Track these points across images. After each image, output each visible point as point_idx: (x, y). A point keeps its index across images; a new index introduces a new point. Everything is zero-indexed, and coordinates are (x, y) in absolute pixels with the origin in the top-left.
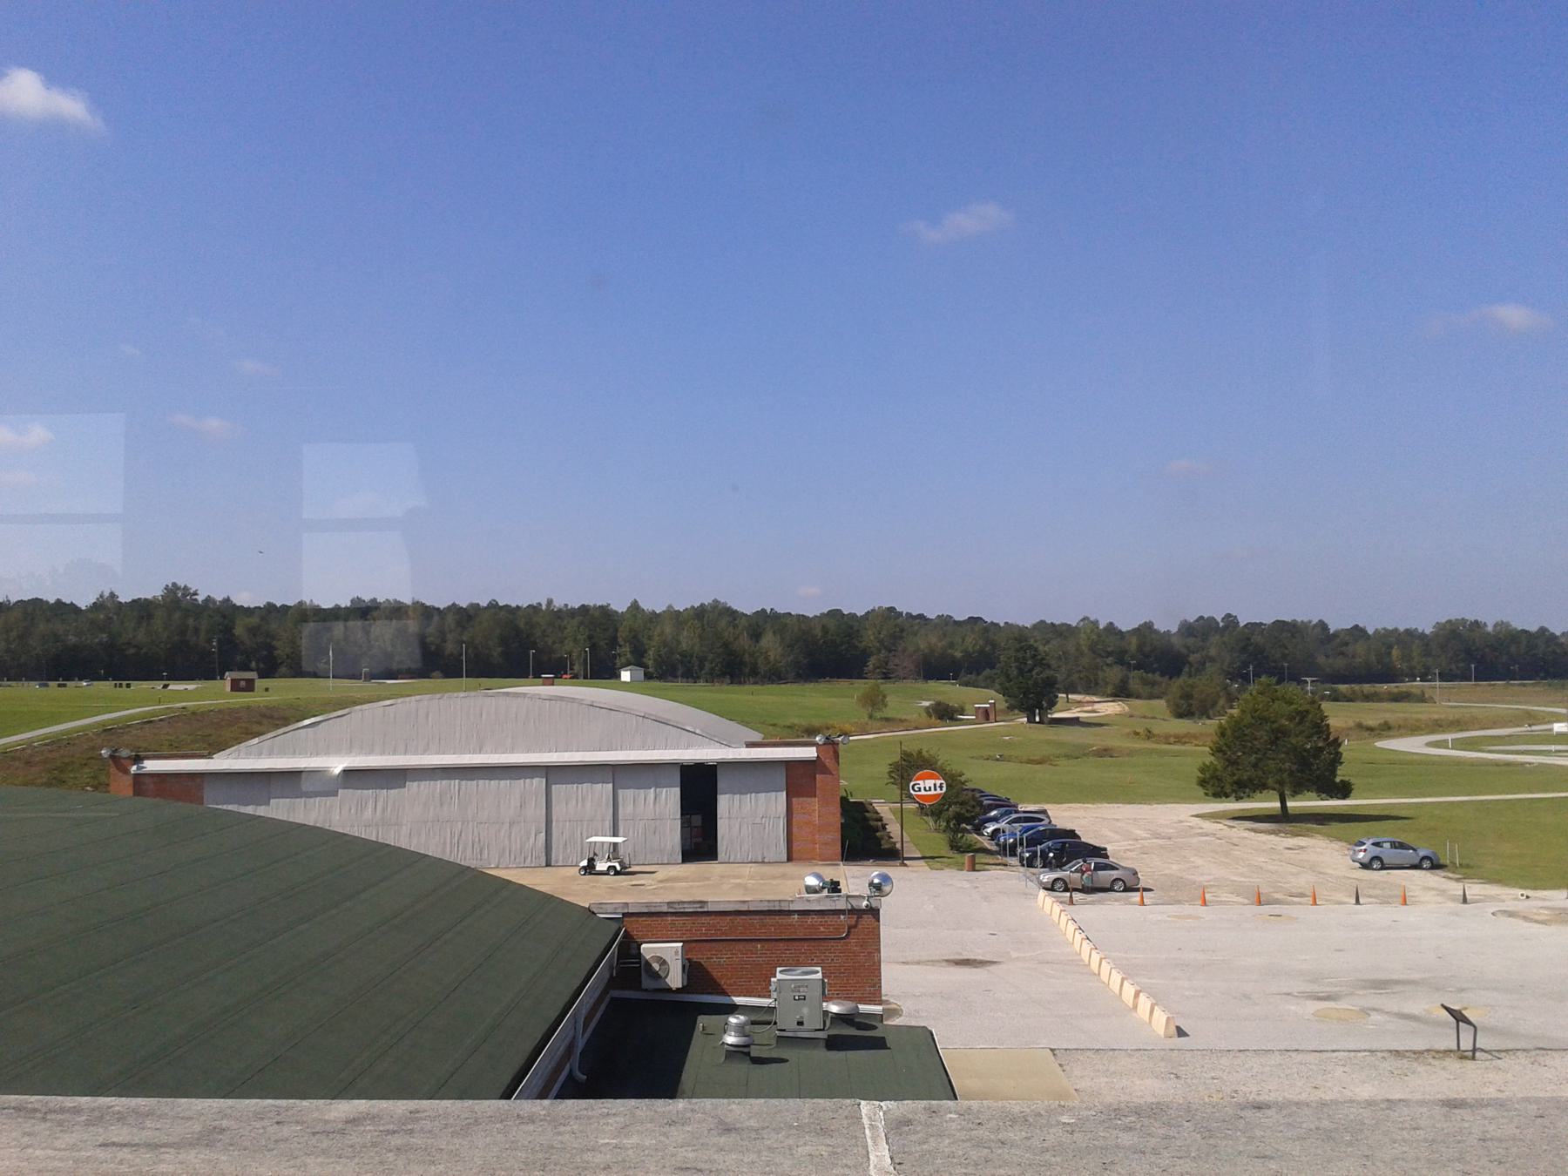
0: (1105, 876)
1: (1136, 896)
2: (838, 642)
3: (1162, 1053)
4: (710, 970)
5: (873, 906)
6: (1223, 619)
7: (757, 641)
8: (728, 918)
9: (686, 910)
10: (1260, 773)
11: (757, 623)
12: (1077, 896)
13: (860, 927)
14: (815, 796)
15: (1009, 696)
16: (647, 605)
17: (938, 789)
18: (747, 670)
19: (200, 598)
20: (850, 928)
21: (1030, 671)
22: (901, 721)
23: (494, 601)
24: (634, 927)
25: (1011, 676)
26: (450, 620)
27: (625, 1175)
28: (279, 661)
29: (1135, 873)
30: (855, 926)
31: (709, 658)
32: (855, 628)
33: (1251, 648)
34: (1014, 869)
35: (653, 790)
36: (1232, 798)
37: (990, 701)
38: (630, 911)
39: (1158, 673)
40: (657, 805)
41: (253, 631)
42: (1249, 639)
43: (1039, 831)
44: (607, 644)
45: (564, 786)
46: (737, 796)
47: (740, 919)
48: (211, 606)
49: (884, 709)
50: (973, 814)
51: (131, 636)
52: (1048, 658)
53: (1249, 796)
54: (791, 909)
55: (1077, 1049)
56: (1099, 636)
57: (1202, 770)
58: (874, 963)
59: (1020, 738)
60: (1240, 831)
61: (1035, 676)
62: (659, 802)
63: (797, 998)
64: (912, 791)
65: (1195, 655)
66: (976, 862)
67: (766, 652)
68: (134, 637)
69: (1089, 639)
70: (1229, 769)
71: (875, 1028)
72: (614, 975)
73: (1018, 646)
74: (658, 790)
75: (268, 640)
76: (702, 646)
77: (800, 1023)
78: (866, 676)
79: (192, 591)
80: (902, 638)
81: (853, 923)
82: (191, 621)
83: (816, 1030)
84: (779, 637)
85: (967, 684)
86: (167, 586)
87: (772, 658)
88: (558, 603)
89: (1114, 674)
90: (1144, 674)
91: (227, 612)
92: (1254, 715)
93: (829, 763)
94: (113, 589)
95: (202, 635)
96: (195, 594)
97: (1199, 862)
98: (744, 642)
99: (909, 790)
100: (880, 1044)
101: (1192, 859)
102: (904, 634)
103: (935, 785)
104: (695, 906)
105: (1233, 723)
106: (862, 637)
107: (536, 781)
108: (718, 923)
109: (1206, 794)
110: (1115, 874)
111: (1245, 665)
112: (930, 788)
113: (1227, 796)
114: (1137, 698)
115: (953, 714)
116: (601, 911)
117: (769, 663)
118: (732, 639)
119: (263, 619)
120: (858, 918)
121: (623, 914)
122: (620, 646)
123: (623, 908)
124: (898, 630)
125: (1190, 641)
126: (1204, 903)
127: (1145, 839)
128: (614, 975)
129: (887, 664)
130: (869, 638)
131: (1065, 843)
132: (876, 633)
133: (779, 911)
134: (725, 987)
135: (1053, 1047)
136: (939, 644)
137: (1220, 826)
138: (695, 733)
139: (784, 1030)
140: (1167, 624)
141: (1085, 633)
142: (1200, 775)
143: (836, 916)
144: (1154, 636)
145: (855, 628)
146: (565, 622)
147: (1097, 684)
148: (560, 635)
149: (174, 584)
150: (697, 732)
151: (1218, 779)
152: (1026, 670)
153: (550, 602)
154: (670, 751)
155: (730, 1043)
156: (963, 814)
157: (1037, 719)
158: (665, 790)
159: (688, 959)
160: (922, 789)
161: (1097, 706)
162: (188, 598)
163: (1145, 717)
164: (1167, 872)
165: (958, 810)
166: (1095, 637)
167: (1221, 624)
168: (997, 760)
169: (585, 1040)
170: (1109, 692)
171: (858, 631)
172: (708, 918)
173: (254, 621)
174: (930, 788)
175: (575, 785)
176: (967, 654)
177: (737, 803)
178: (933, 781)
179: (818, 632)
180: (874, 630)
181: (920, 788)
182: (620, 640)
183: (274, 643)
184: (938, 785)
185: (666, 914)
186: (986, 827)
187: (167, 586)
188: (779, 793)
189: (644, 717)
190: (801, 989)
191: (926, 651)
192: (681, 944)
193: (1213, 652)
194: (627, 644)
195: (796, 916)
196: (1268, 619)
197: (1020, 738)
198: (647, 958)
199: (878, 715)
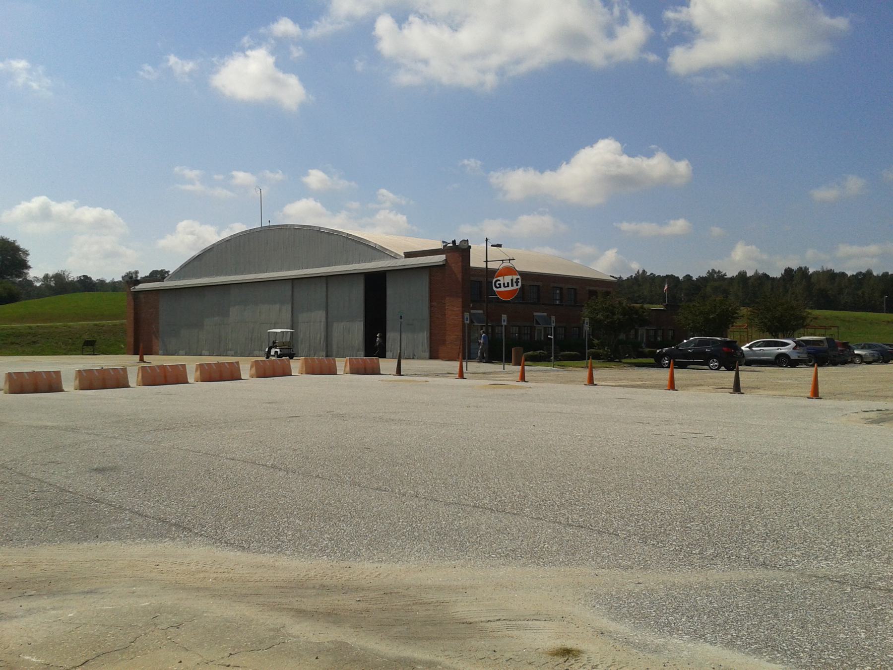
17: (515, 284)
27: (525, 669)
64: (495, 289)
86: (709, 271)
94: (644, 269)
103: (512, 280)
112: (508, 283)
149: (713, 270)
154: (355, 265)
160: (502, 285)
174: (508, 283)
178: (510, 277)
181: (500, 284)
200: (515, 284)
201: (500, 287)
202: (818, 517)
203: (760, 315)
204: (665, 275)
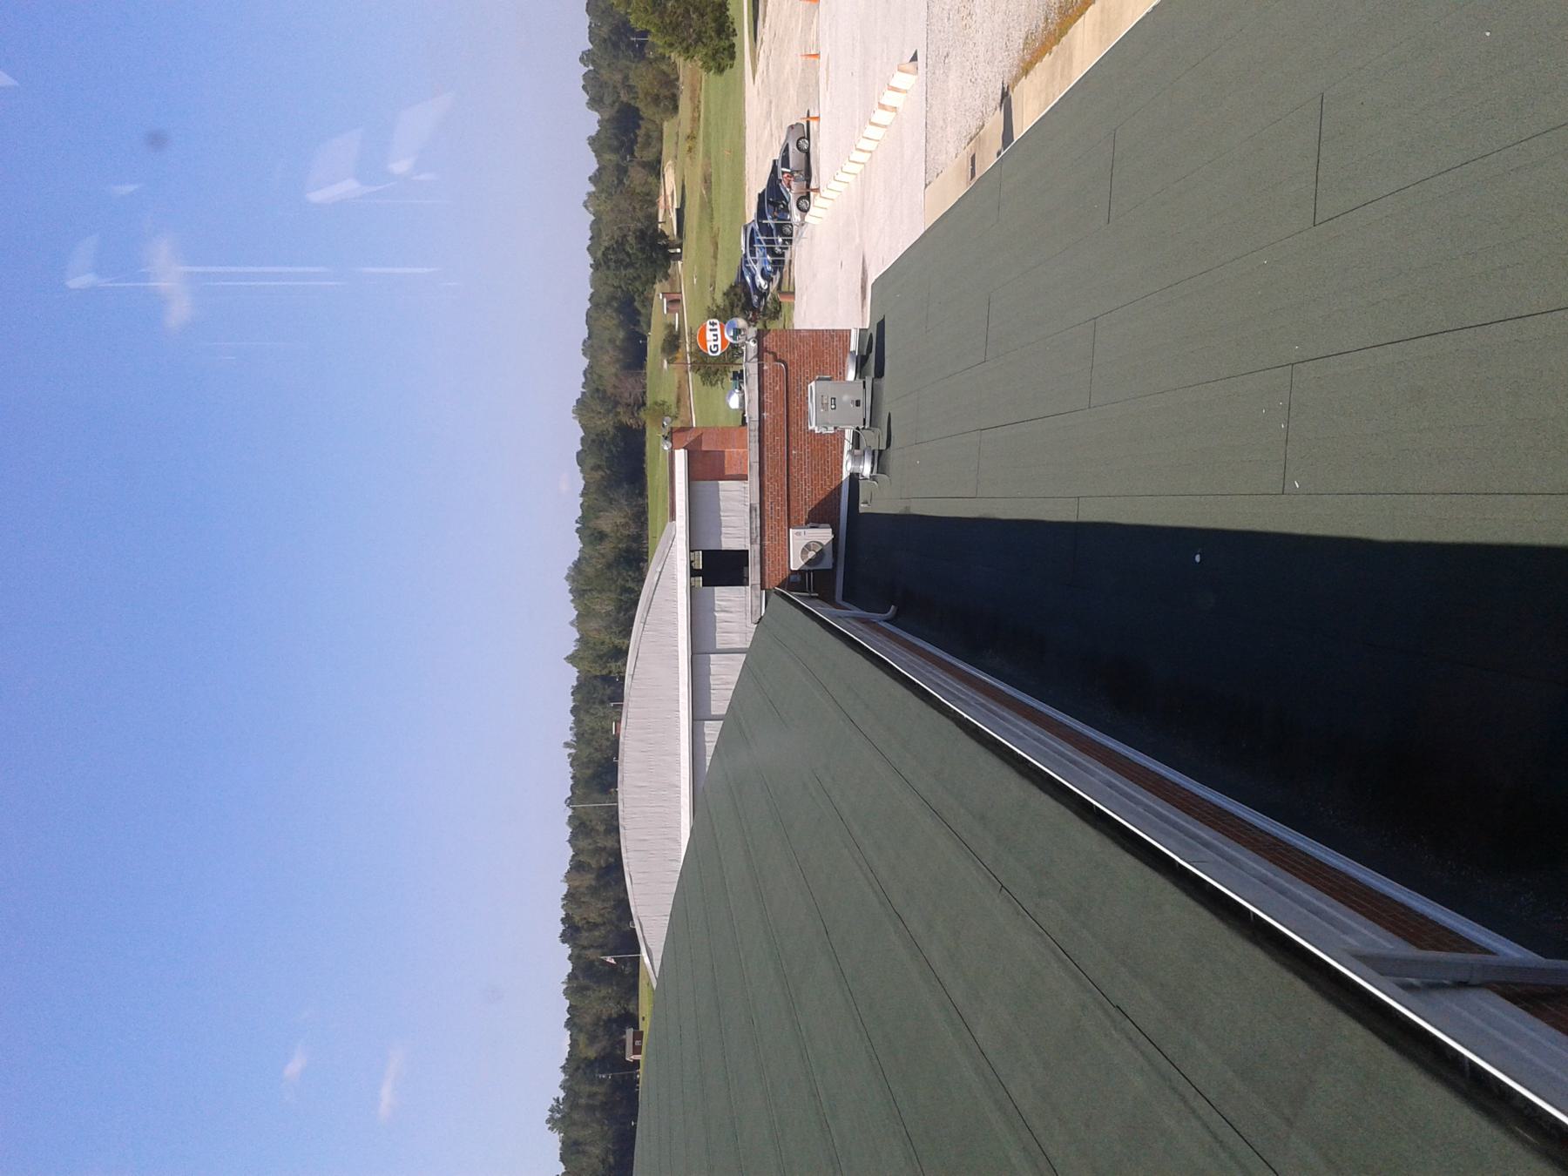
0: (795, 158)
1: (813, 124)
2: (607, 455)
3: (929, 75)
4: (817, 502)
5: (754, 336)
6: (585, 65)
7: (606, 536)
8: (767, 483)
9: (759, 525)
10: (709, 9)
11: (590, 536)
12: (813, 186)
13: (775, 350)
14: (723, 452)
15: (655, 277)
16: (571, 648)
17: (715, 327)
18: (634, 545)
19: (562, 1094)
20: (776, 359)
21: (628, 255)
22: (679, 387)
23: (566, 801)
24: (775, 579)
25: (635, 275)
26: (584, 843)
28: (623, 1012)
29: (792, 127)
30: (775, 354)
31: (623, 583)
32: (595, 437)
33: (613, 38)
34: (793, 253)
35: (716, 614)
36: (735, 40)
37: (661, 297)
38: (759, 582)
39: (637, 131)
40: (733, 610)
41: (592, 1039)
42: (605, 40)
43: (760, 229)
44: (609, 687)
45: (712, 702)
46: (724, 530)
47: (767, 473)
48: (569, 1084)
49: (668, 404)
50: (743, 295)
51: (597, 1160)
52: (616, 237)
53: (732, 23)
54: (757, 419)
55: (926, 161)
56: (602, 191)
57: (708, 70)
58: (810, 336)
59: (696, 268)
60: (765, 33)
61: (635, 251)
62: (731, 607)
63: (833, 407)
64: (718, 354)
65: (622, 95)
66: (787, 290)
67: (617, 526)
68: (597, 1157)
69: (605, 202)
70: (704, 40)
71: (871, 335)
72: (817, 595)
73: (605, 268)
74: (716, 609)
75: (602, 1023)
76: (610, 591)
77: (858, 403)
78: (641, 428)
79: (555, 1104)
80: (605, 391)
81: (771, 356)
82: (583, 1101)
83: (864, 387)
84: (602, 513)
85: (649, 326)
87: (623, 520)
88: (569, 737)
89: (637, 176)
90: (638, 145)
91: (576, 1067)
92: (650, 13)
93: (690, 437)
95: (595, 1089)
96: (557, 1100)
97: (788, 67)
98: (607, 548)
99: (719, 357)
100: (881, 326)
101: (786, 76)
102: (601, 388)
103: (711, 330)
104: (754, 516)
105: (659, 34)
106: (603, 431)
107: (706, 731)
108: (771, 493)
109: (731, 67)
110: (792, 147)
111: (630, 45)
112: (714, 335)
113: (733, 46)
114: (661, 154)
115: (674, 336)
116: (759, 612)
117: (627, 523)
118: (604, 560)
119: (581, 1030)
120: (767, 351)
121: (762, 589)
122: (610, 672)
123: (756, 589)
124: (596, 395)
125: (608, 100)
126: (817, 55)
127: (771, 125)
128: (817, 595)
129: (629, 405)
130: (605, 424)
131: (768, 200)
132: (599, 416)
133: (760, 431)
134: (833, 487)
135: (924, 186)
136: (611, 352)
137: (761, 52)
138: (660, 573)
139: (864, 420)
140: (591, 122)
141: (599, 205)
142: (713, 71)
143: (765, 374)
144: (602, 136)
145: (595, 437)
146: (587, 728)
147: (648, 194)
148: (600, 734)
149: (548, 1121)
150: (659, 570)
151: (716, 52)
152: (628, 260)
153: (567, 745)
155: (870, 470)
156: (743, 304)
157: (679, 250)
158: (716, 602)
159: (806, 524)
160: (715, 343)
161: (668, 193)
162: (561, 1107)
163: (677, 143)
164: (795, 98)
165: (739, 309)
166: (603, 195)
167: (591, 68)
168: (714, 289)
169: (851, 606)
170: (656, 181)
171: (597, 435)
172: (767, 503)
173: (582, 1039)
174: (714, 335)
175: (712, 691)
176: (621, 325)
177: (730, 530)
179: (598, 475)
180: (596, 418)
181: (715, 346)
182: (604, 673)
183: (604, 1017)
184: (711, 327)
185: (762, 546)
186: (760, 286)
187: (549, 1128)
188: (720, 487)
189: (645, 624)
190: (825, 402)
191: (618, 366)
192: (791, 530)
193: (618, 77)
194: (608, 665)
195: (765, 414)
196: (586, 20)
197: (696, 268)
198: (803, 563)
199: (674, 410)
200: (715, 327)
201: (717, 345)
202: (1346, 294)
203: (623, 583)
204: (579, 468)
